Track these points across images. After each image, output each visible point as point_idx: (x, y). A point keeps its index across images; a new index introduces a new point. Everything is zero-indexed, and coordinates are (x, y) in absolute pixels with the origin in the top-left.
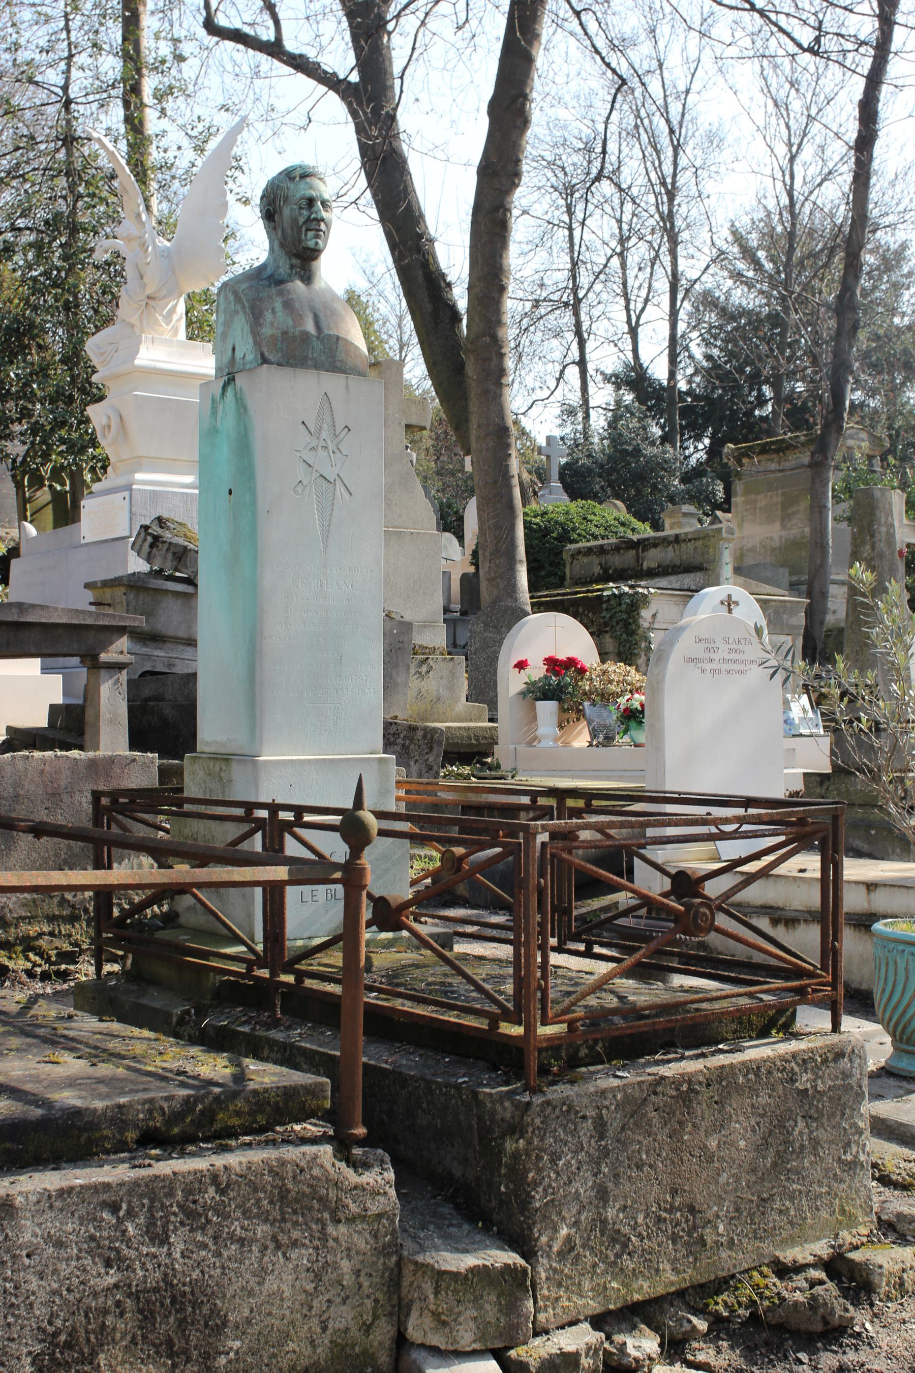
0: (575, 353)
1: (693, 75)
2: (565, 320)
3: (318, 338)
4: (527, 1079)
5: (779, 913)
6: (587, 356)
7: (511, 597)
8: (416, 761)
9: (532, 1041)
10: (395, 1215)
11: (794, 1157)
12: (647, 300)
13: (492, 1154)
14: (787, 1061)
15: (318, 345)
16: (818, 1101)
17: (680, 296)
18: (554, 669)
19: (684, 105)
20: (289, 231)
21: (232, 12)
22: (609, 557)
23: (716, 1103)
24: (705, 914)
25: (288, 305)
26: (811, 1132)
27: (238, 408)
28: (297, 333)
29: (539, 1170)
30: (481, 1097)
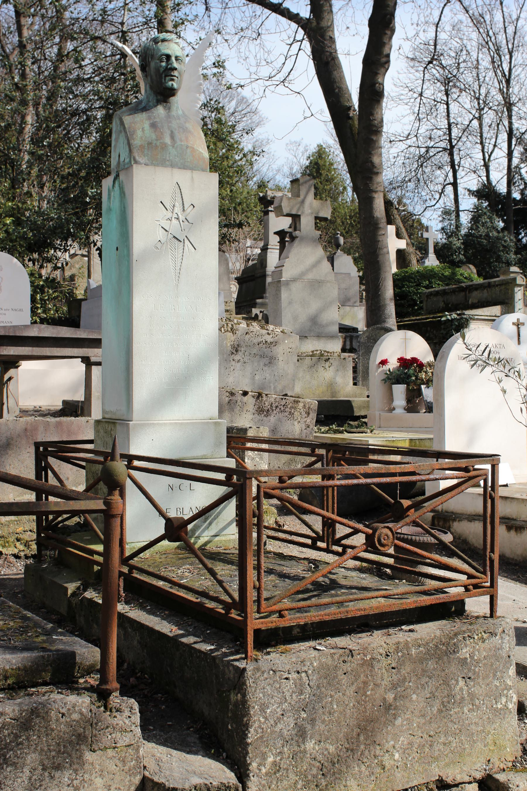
0: (451, 179)
1: (521, 8)
2: (445, 159)
4: (246, 653)
5: (513, 522)
6: (458, 181)
12: (495, 146)
14: (451, 638)
17: (514, 142)
19: (516, 27)
23: (393, 668)
27: (121, 194)
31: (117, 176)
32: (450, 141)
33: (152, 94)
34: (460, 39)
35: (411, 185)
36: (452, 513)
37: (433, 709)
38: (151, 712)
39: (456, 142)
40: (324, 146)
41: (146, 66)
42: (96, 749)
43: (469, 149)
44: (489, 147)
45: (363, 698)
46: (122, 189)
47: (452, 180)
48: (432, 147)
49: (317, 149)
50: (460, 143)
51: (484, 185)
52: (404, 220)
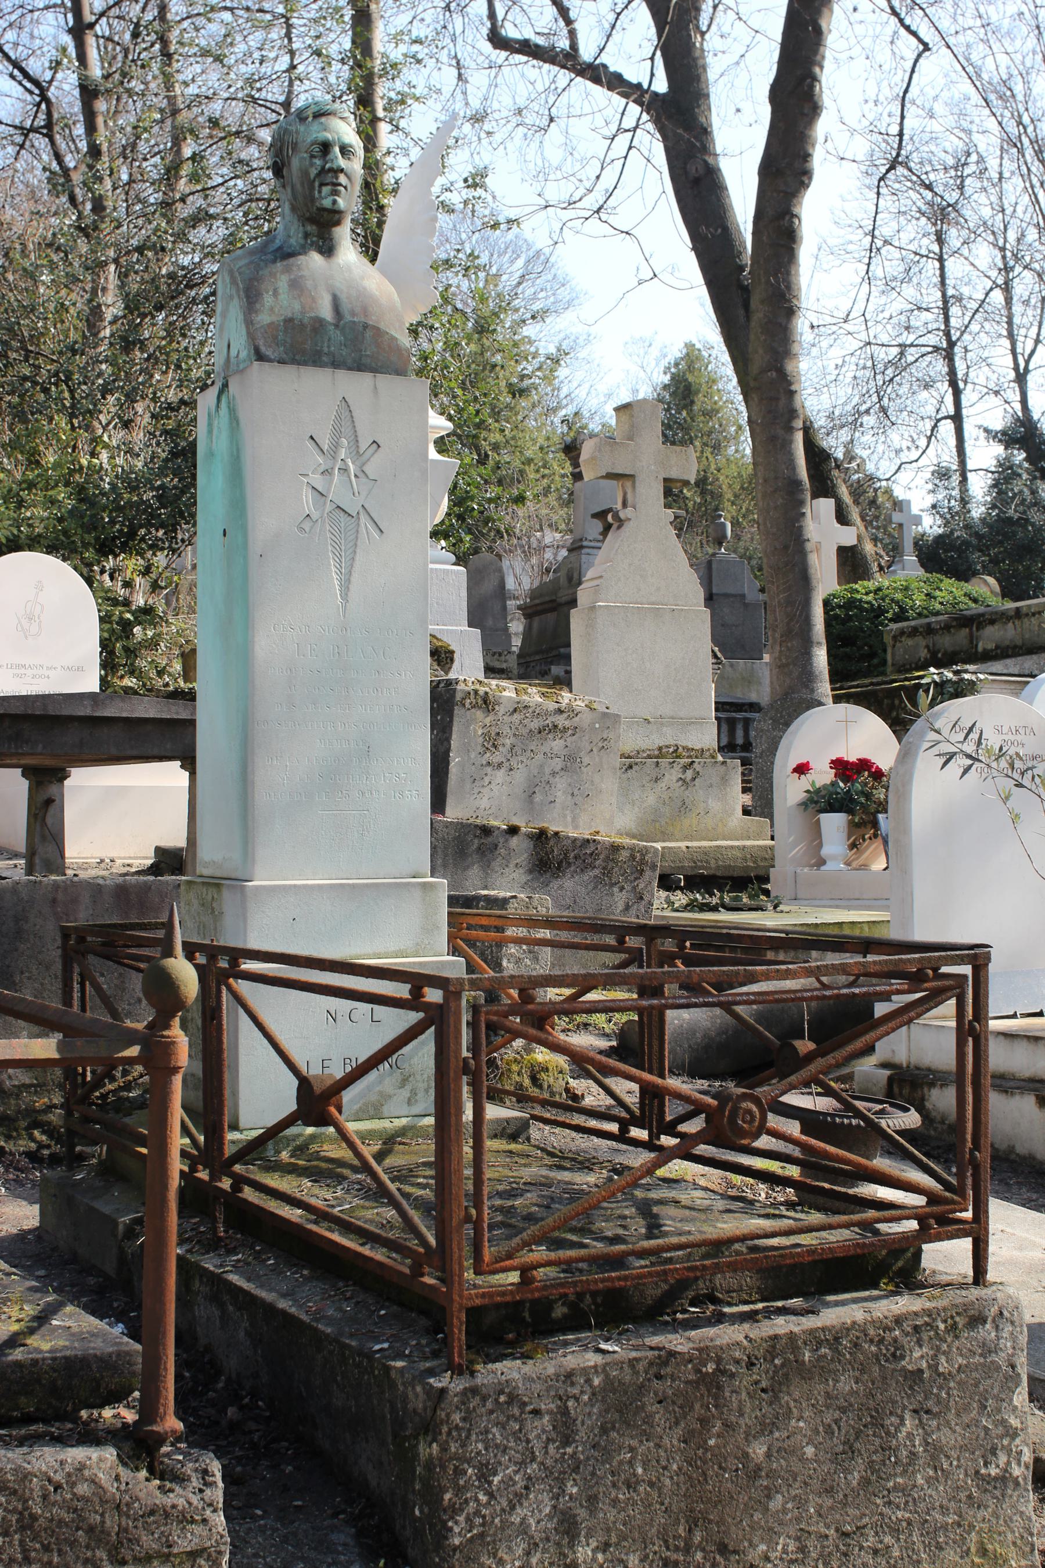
0: (949, 408)
3: (337, 326)
6: (964, 412)
7: (807, 687)
8: (622, 889)
9: (456, 1297)
10: (220, 1553)
11: (899, 1470)
12: (1037, 341)
13: (406, 1457)
14: (887, 1329)
15: (337, 336)
16: (940, 1388)
18: (843, 774)
20: (299, 187)
21: (520, 19)
22: (937, 638)
23: (763, 1390)
24: (749, 1112)
25: (296, 285)
26: (927, 1434)
27: (231, 423)
28: (306, 321)
29: (459, 1490)
30: (393, 1374)
31: (225, 385)
32: (947, 334)
33: (296, 221)
34: (963, 130)
35: (869, 420)
36: (929, 1070)
37: (849, 1477)
38: (264, 1478)
39: (958, 334)
40: (698, 346)
41: (283, 165)
42: (128, 1557)
43: (984, 348)
44: (1025, 346)
45: (700, 1452)
46: (232, 412)
47: (952, 411)
48: (912, 345)
49: (684, 351)
50: (966, 337)
51: (1018, 419)
52: (857, 491)
